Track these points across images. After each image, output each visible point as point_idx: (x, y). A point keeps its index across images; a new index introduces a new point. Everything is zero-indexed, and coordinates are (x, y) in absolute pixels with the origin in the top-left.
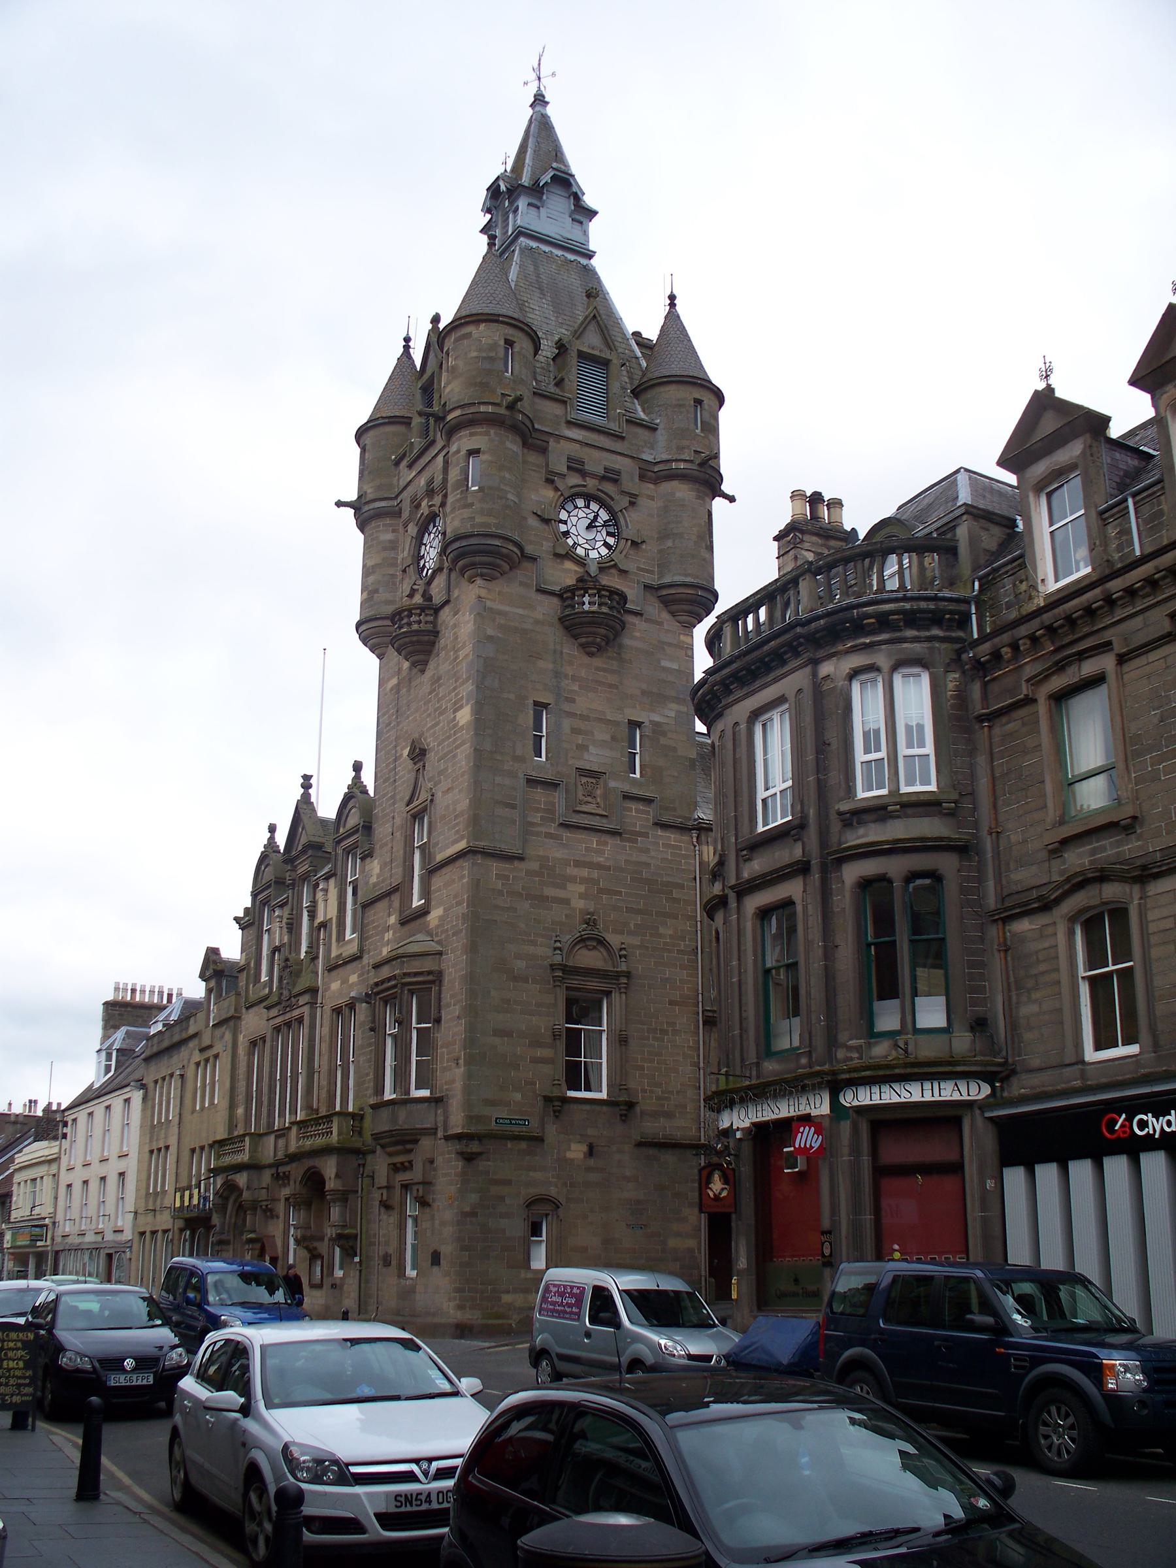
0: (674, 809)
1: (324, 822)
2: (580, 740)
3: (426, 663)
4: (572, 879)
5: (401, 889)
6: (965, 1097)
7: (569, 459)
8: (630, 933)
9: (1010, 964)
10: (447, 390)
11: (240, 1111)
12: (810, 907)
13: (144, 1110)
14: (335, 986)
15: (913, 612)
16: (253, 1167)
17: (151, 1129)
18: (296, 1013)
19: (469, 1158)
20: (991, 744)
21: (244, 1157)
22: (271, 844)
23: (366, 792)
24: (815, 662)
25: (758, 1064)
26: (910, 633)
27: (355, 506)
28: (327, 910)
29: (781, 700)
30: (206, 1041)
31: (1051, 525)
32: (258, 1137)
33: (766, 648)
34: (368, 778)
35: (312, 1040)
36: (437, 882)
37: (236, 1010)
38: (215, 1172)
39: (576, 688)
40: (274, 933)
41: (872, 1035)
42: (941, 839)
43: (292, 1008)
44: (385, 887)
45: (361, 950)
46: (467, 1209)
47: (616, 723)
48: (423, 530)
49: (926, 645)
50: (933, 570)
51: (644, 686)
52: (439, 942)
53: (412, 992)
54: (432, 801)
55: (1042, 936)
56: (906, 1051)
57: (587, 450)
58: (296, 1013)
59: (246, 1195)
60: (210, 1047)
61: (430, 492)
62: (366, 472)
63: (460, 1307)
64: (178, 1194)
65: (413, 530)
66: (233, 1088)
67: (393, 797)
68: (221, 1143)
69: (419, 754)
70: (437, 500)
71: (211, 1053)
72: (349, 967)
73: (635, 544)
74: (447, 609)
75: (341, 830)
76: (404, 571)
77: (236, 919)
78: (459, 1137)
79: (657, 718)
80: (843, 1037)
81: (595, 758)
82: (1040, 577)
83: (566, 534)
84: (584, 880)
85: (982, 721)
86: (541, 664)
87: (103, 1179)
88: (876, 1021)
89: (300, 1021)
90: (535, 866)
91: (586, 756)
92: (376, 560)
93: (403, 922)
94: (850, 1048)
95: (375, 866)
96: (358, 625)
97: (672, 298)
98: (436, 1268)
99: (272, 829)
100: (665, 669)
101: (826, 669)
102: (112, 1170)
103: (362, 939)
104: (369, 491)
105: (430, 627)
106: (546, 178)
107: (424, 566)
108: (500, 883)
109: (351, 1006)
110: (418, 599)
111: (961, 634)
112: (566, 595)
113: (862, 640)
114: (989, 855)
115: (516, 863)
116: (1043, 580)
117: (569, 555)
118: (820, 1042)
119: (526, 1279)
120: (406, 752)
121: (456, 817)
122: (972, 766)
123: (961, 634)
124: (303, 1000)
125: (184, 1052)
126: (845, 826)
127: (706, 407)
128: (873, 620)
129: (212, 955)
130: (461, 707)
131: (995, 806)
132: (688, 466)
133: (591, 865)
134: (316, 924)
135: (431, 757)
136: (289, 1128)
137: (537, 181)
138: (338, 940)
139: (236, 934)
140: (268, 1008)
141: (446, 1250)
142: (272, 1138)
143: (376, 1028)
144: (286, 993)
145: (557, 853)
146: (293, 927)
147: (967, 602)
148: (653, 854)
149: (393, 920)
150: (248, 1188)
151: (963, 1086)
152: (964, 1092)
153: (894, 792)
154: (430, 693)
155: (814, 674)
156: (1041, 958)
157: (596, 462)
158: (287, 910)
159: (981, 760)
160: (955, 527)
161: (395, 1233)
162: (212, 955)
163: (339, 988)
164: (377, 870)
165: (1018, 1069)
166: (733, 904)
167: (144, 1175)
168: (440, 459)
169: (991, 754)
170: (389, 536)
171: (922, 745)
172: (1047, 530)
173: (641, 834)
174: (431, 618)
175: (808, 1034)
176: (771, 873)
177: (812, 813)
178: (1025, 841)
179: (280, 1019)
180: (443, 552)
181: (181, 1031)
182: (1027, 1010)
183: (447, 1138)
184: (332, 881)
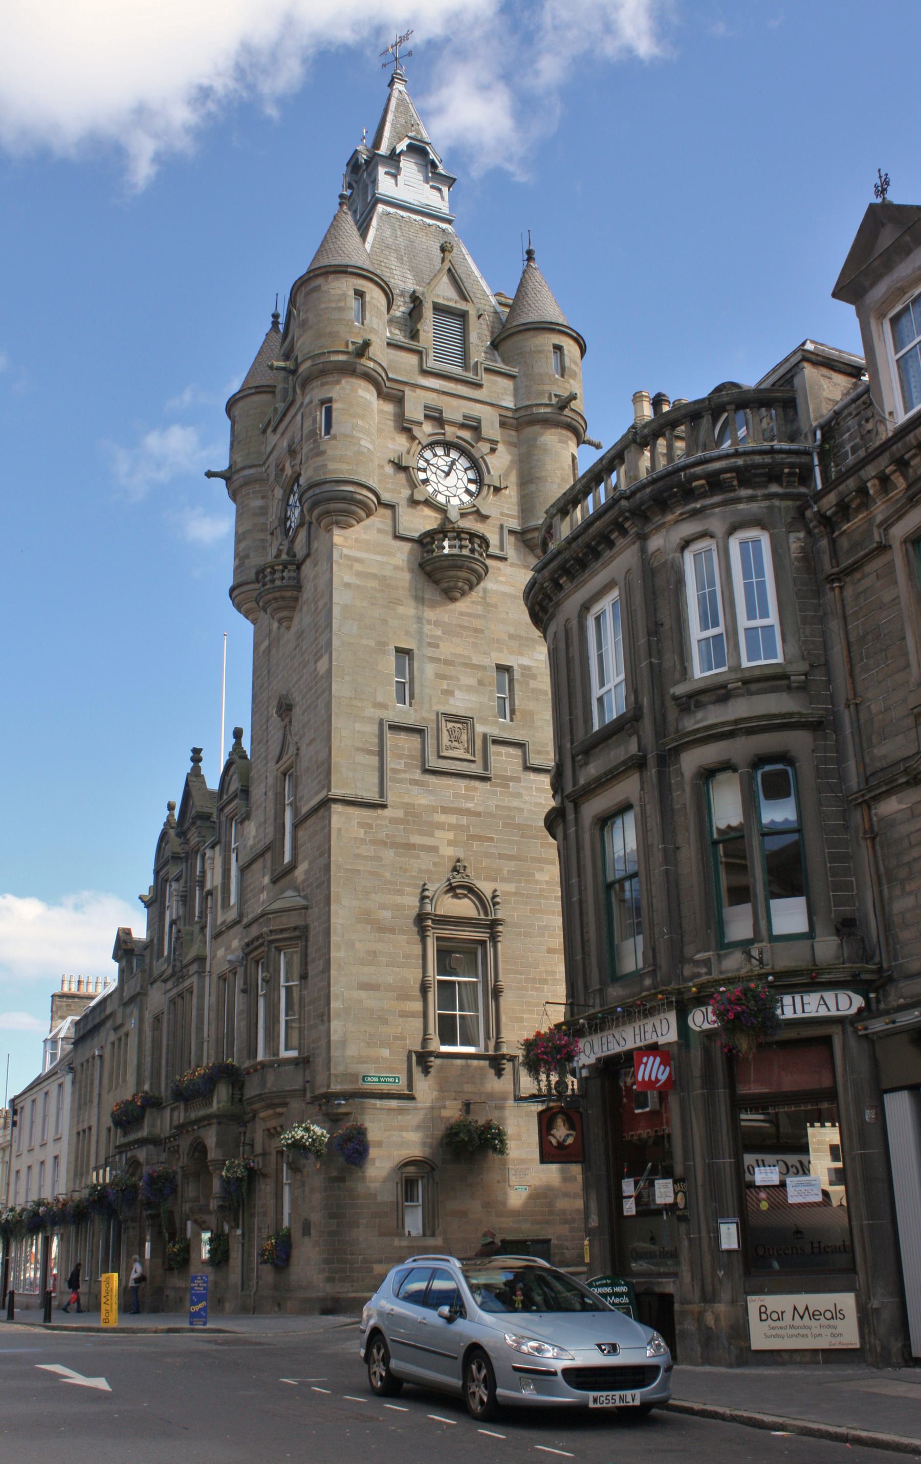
1: (212, 793)
3: (291, 619)
4: (440, 826)
5: (273, 848)
6: (834, 1013)
7: (426, 407)
8: (504, 880)
9: (879, 854)
12: (648, 807)
14: (220, 953)
15: (747, 468)
18: (187, 983)
20: (843, 607)
23: (245, 757)
24: (643, 538)
25: (601, 991)
26: (744, 492)
27: (227, 476)
30: (119, 1021)
31: (896, 352)
33: (592, 530)
37: (142, 987)
39: (439, 633)
41: (723, 946)
42: (791, 715)
43: (183, 978)
44: (260, 847)
46: (335, 1174)
47: (483, 668)
48: (289, 492)
49: (765, 504)
50: (772, 430)
51: (512, 630)
52: (305, 897)
53: (279, 950)
55: (913, 816)
56: (761, 961)
60: (122, 1025)
62: (235, 443)
63: (330, 1280)
65: (279, 493)
67: (266, 757)
73: (497, 490)
75: (225, 797)
76: (272, 534)
79: (525, 661)
80: (689, 950)
81: (460, 703)
82: (887, 409)
84: (452, 827)
85: (833, 581)
86: (401, 609)
88: (727, 930)
90: (400, 814)
91: (451, 701)
93: (274, 881)
94: (697, 963)
96: (232, 590)
98: (306, 1239)
101: (655, 543)
104: (238, 460)
105: (293, 583)
106: (402, 146)
107: (290, 526)
108: (362, 831)
111: (803, 490)
112: (426, 541)
113: (693, 506)
114: (848, 731)
115: (380, 812)
116: (891, 414)
118: (663, 960)
119: (400, 1247)
121: (318, 768)
122: (824, 634)
123: (803, 490)
124: (194, 968)
125: (103, 1032)
126: (681, 711)
127: (566, 352)
128: (702, 482)
130: (321, 656)
131: (852, 674)
132: (548, 410)
135: (297, 711)
137: (394, 149)
138: (223, 907)
140: (165, 981)
141: (316, 1218)
143: (249, 990)
144: (178, 964)
145: (422, 799)
147: (807, 453)
148: (526, 798)
149: (266, 880)
150: (148, 1163)
151: (829, 996)
152: (832, 1006)
153: (737, 668)
154: (295, 649)
155: (643, 550)
156: (913, 842)
157: (454, 410)
159: (835, 625)
160: (792, 377)
161: (271, 1202)
164: (253, 831)
165: (895, 975)
166: (571, 816)
168: (299, 417)
169: (845, 617)
170: (258, 503)
171: (765, 614)
172: (893, 357)
173: (511, 779)
174: (294, 574)
175: (652, 951)
176: (606, 774)
177: (646, 701)
178: (887, 709)
181: (100, 1013)
182: (901, 905)
184: (217, 848)
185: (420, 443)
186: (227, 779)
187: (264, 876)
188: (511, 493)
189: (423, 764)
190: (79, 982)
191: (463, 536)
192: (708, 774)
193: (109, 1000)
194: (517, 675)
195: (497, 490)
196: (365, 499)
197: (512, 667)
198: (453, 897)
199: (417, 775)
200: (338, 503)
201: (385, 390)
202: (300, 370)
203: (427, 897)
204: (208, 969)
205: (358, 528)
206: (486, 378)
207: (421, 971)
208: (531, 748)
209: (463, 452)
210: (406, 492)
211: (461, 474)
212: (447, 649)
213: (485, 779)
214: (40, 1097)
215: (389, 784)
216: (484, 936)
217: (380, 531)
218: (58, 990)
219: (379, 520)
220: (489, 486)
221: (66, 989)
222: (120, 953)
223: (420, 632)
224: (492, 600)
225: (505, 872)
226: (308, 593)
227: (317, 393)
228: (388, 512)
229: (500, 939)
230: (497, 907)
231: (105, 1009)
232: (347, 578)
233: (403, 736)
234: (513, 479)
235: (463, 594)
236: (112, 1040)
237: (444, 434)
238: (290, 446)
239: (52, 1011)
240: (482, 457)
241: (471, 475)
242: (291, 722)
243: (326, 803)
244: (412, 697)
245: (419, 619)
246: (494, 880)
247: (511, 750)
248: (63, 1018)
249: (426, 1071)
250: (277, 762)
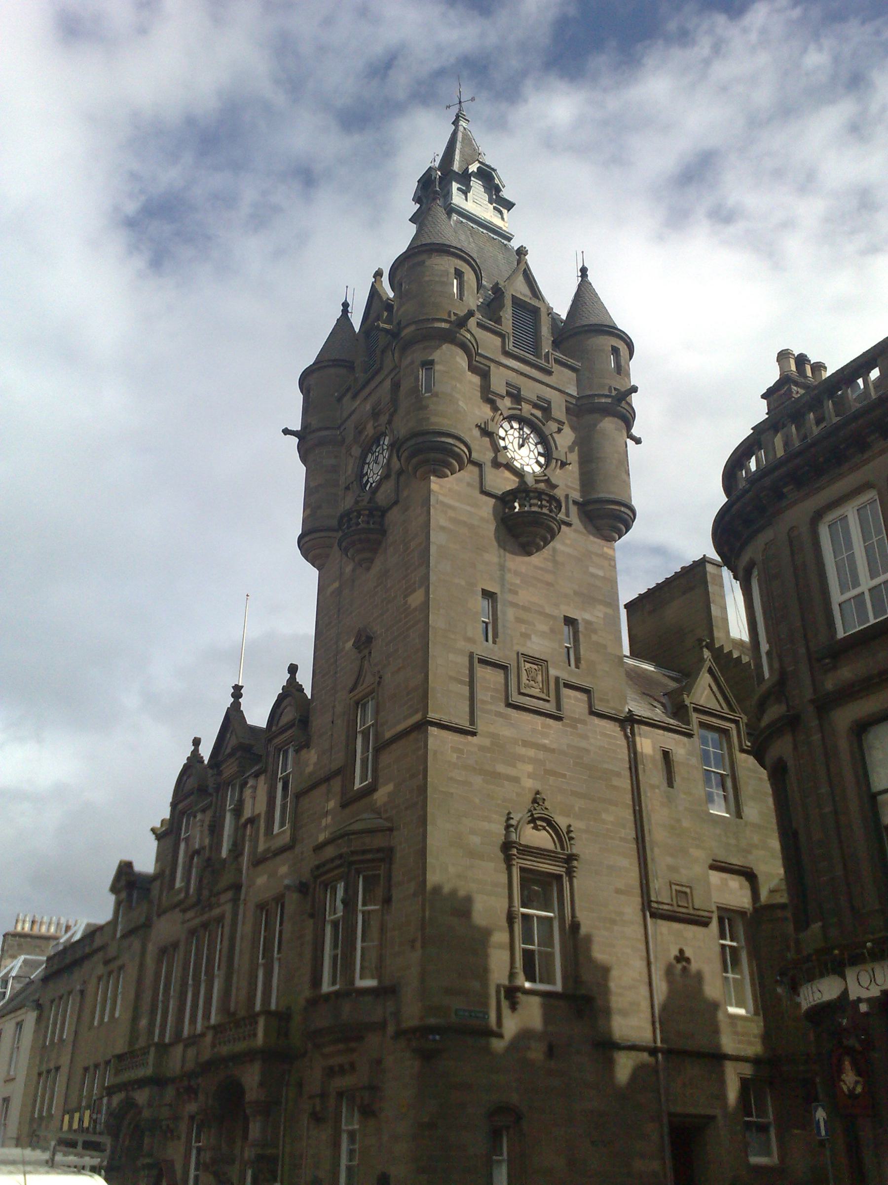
0: (608, 701)
2: (523, 628)
3: (372, 561)
4: (521, 758)
5: (345, 772)
10: (400, 313)
11: (144, 1022)
13: (36, 1031)
16: (158, 1082)
17: (42, 1050)
18: (216, 912)
19: (427, 1056)
21: (147, 1071)
22: (195, 757)
30: (112, 951)
32: (163, 1048)
34: (305, 679)
35: (232, 939)
36: (386, 758)
38: (110, 1091)
40: (196, 834)
43: (211, 907)
45: (294, 840)
48: (367, 450)
52: (386, 819)
53: (358, 872)
54: (379, 683)
57: (522, 378)
58: (216, 912)
59: (146, 1114)
61: (375, 414)
64: (67, 1117)
65: (356, 451)
66: (138, 996)
68: (120, 1057)
69: (364, 641)
70: (384, 419)
71: (114, 966)
72: (278, 859)
74: (395, 509)
75: (274, 728)
76: (347, 488)
77: (153, 830)
78: (414, 1030)
79: (587, 616)
81: (537, 646)
83: (505, 448)
86: (487, 556)
89: (220, 919)
90: (487, 742)
91: (529, 644)
93: (344, 806)
95: (312, 756)
99: (197, 742)
100: (593, 575)
103: (295, 828)
107: (368, 481)
108: (455, 755)
109: (279, 900)
112: (504, 500)
117: (509, 467)
120: (350, 644)
124: (224, 898)
125: (87, 966)
129: (125, 869)
130: (414, 591)
134: (243, 820)
136: (203, 1035)
139: (152, 845)
140: (184, 911)
142: (180, 1048)
145: (507, 732)
146: (215, 829)
149: (331, 804)
157: (531, 390)
158: (209, 814)
162: (125, 869)
163: (261, 884)
179: (197, 921)
183: (400, 1034)
184: (262, 778)
185: (501, 414)
186: (279, 711)
187: (328, 801)
188: (573, 468)
189: (507, 698)
190: (33, 922)
191: (543, 497)
193: (98, 933)
194: (581, 628)
195: (563, 464)
196: (462, 453)
197: (576, 620)
198: (533, 828)
199: (501, 708)
200: (433, 453)
201: (474, 363)
202: (403, 334)
203: (512, 826)
204: (242, 897)
205: (451, 478)
206: (556, 368)
207: (507, 900)
208: (596, 695)
209: (535, 429)
210: (491, 455)
211: (532, 447)
212: (525, 596)
213: (559, 719)
215: (478, 713)
216: (559, 870)
217: (469, 484)
218: (11, 929)
219: (469, 474)
220: (557, 460)
221: (19, 928)
222: (123, 883)
223: (502, 579)
224: (560, 559)
225: (577, 809)
227: (417, 355)
228: (476, 470)
229: (575, 874)
230: (572, 842)
231: (93, 941)
232: (443, 522)
233: (489, 670)
234: (573, 457)
235: (539, 549)
236: (99, 973)
237: (520, 410)
238: (374, 409)
239: (3, 950)
240: (551, 434)
241: (540, 448)
242: (370, 653)
243: (423, 725)
244: (495, 635)
245: (502, 568)
246: (568, 816)
247: (578, 694)
248: (14, 957)
249: (513, 1007)
250: (351, 691)
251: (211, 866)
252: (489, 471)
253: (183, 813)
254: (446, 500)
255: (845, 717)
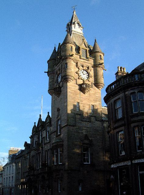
4: (84, 129)
5: (56, 131)
14: (46, 147)
17: (17, 169)
24: (125, 92)
28: (44, 135)
29: (119, 99)
34: (50, 115)
40: (36, 139)
53: (58, 148)
61: (59, 70)
65: (57, 76)
69: (58, 110)
79: (96, 104)
84: (85, 130)
87: (10, 177)
92: (51, 81)
93: (57, 137)
95: (52, 128)
97: (95, 40)
99: (35, 123)
101: (127, 93)
102: (11, 175)
103: (50, 140)
110: (58, 86)
129: (26, 143)
133: (86, 127)
139: (30, 139)
140: (35, 151)
143: (53, 153)
146: (39, 138)
149: (55, 136)
155: (125, 94)
162: (26, 143)
167: (16, 177)
180: (62, 78)
184: (45, 131)
192: (135, 127)
213: (90, 122)
214: (9, 167)
226: (62, 92)
232: (69, 91)
251: (38, 144)
252: (78, 80)
253: (34, 135)
254: (70, 87)
255: (132, 125)
